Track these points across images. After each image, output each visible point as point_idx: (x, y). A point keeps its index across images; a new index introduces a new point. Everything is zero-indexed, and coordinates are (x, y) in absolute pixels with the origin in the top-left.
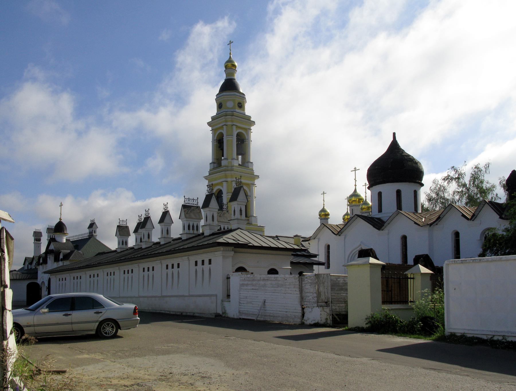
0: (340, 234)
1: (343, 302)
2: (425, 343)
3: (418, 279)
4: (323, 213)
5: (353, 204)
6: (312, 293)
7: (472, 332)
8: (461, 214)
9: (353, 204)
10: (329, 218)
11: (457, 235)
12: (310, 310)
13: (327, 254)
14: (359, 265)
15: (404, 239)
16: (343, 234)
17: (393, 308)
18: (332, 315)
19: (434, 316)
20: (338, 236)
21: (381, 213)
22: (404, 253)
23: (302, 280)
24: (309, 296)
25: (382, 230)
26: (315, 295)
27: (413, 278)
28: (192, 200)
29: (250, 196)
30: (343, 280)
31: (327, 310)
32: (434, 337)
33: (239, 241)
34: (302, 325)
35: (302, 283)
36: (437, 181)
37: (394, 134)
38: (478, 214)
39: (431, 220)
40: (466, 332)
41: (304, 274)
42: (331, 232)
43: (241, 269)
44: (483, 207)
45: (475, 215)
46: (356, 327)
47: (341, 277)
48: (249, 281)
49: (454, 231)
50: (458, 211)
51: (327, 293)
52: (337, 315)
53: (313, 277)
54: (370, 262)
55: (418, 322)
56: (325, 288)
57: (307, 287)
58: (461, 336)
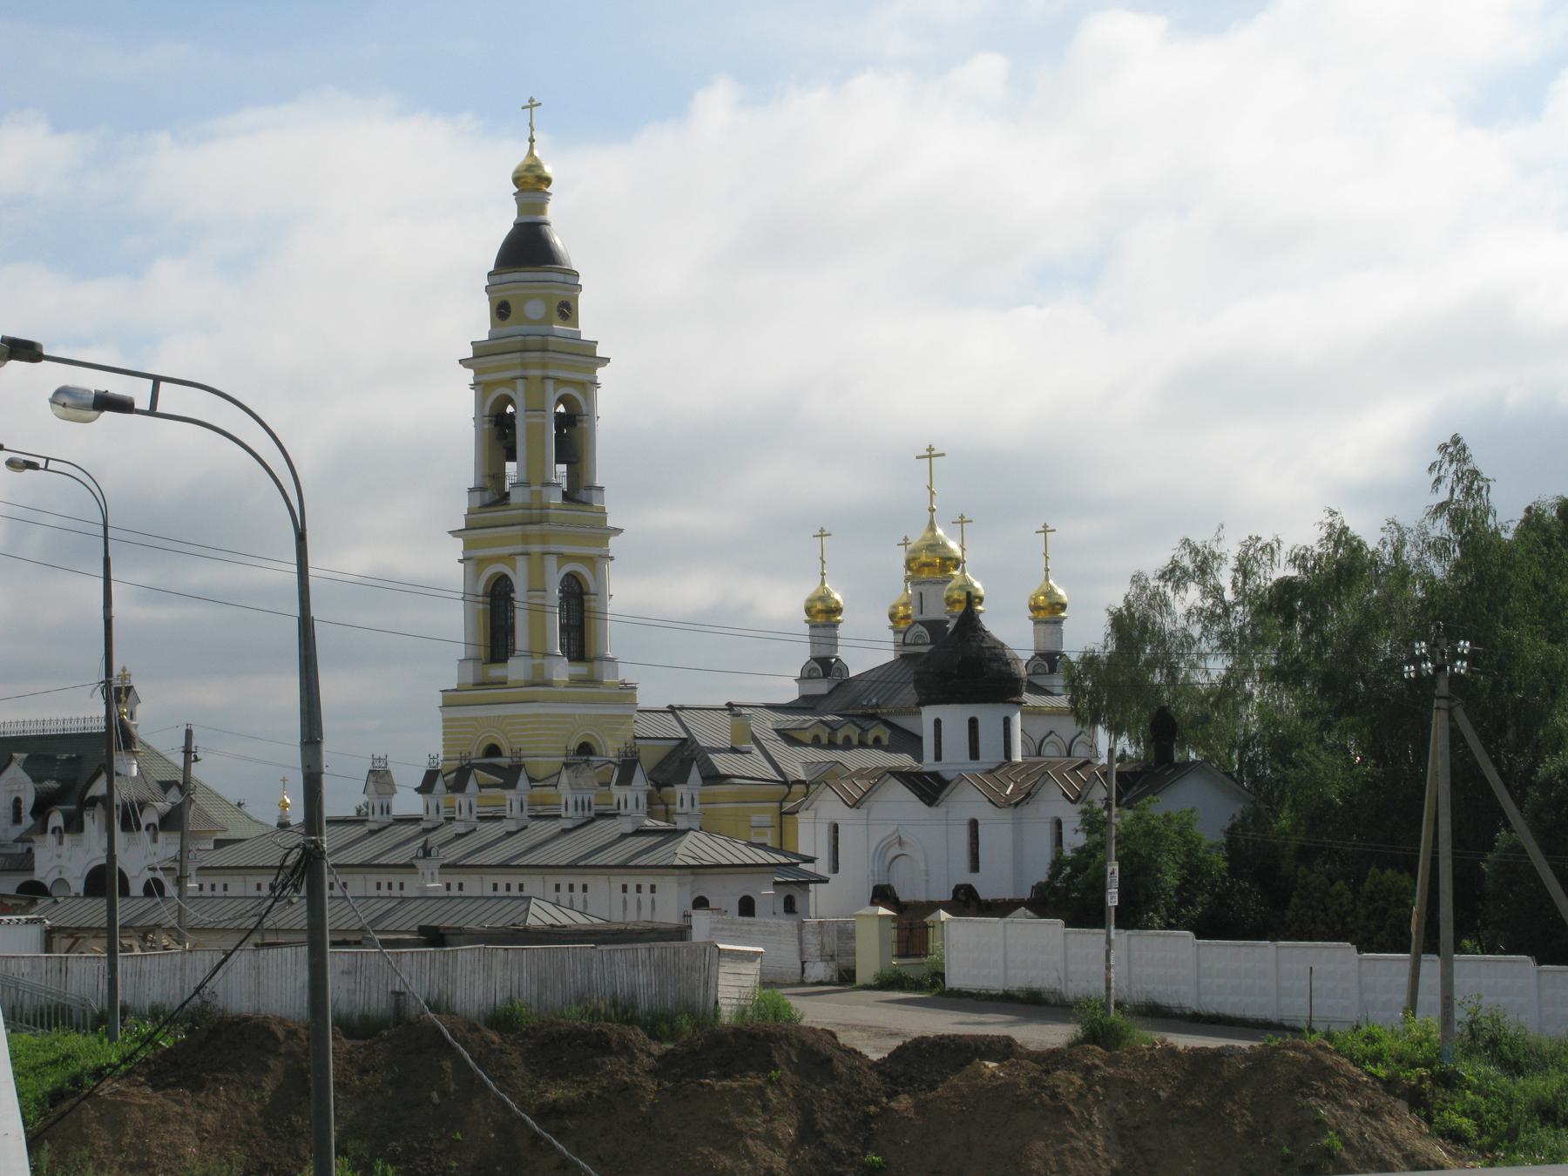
0: (858, 805)
5: (923, 576)
9: (923, 576)
12: (811, 965)
13: (832, 841)
14: (868, 916)
15: (974, 825)
18: (839, 971)
20: (854, 809)
25: (937, 806)
26: (818, 947)
29: (596, 594)
31: (833, 965)
33: (702, 859)
34: (802, 983)
43: (701, 903)
51: (832, 943)
52: (844, 971)
57: (808, 936)
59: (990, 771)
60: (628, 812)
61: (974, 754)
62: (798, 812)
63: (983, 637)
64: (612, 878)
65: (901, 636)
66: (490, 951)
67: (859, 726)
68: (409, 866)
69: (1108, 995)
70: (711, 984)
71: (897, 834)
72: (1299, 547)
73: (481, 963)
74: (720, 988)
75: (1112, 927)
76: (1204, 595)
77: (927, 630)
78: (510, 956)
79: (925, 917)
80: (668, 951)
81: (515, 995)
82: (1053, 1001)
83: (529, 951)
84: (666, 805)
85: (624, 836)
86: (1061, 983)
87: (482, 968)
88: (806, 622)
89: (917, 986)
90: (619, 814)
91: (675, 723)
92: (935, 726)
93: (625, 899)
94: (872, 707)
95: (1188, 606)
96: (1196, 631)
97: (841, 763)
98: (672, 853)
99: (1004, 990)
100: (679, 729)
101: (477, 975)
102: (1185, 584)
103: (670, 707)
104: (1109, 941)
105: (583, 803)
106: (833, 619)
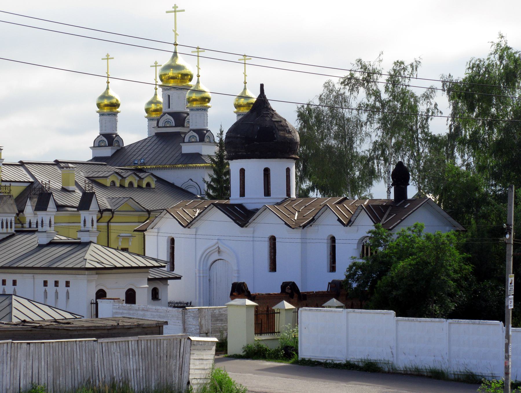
0: (189, 226)
1: (219, 332)
2: (284, 365)
3: (283, 313)
4: (106, 102)
6: (195, 325)
7: (316, 358)
8: (337, 218)
10: (118, 112)
11: (333, 239)
14: (237, 306)
15: (273, 240)
16: (194, 226)
17: (263, 338)
19: (293, 345)
20: (187, 229)
21: (244, 198)
22: (273, 257)
23: (184, 314)
24: (191, 328)
25: (246, 227)
27: (279, 313)
28: (4, 188)
30: (218, 311)
32: (291, 361)
35: (184, 316)
36: (331, 84)
37: (262, 86)
38: (355, 219)
39: (305, 217)
40: (312, 357)
41: (187, 308)
42: (178, 222)
44: (360, 212)
45: (351, 221)
46: (234, 355)
47: (216, 309)
48: (125, 310)
49: (330, 235)
50: (333, 213)
53: (196, 312)
54: (247, 304)
55: (281, 350)
56: (206, 321)
57: (189, 320)
58: (308, 360)
59: (278, 204)
60: (44, 229)
61: (267, 193)
62: (146, 230)
63: (273, 114)
64: (36, 276)
65: (155, 122)
66: (16, 345)
67: (138, 176)
68: (189, 317)
69: (507, 379)
70: (185, 368)
71: (217, 246)
72: (475, 59)
73: (9, 355)
74: (191, 371)
75: (511, 325)
76: (369, 95)
77: (173, 118)
78: (32, 349)
79: (273, 307)
80: (152, 341)
81: (35, 381)
82: (387, 369)
83: (45, 344)
84: (22, 224)
85: (41, 247)
86: (393, 357)
87: (9, 359)
88: (98, 112)
89: (274, 356)
90: (37, 231)
91: (25, 172)
92: (287, 172)
93: (46, 291)
94: (141, 164)
95: (358, 103)
96: (364, 117)
97: (132, 198)
98: (82, 259)
99: (347, 361)
100: (28, 176)
101: (5, 364)
102: (357, 88)
103: (21, 162)
104: (508, 337)
105: (7, 223)
106: (114, 110)
